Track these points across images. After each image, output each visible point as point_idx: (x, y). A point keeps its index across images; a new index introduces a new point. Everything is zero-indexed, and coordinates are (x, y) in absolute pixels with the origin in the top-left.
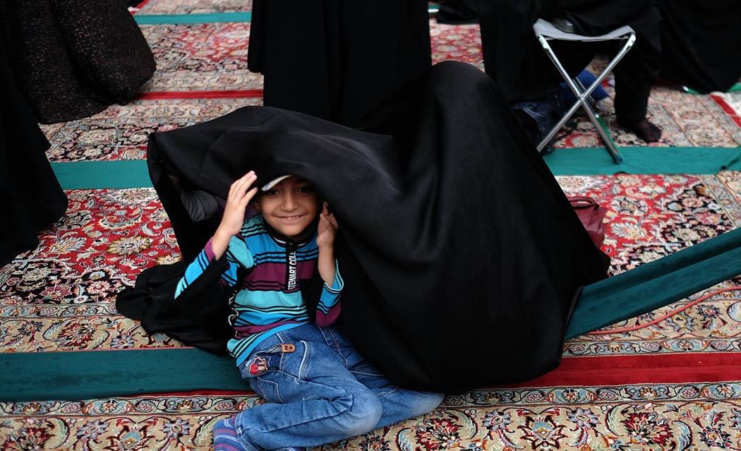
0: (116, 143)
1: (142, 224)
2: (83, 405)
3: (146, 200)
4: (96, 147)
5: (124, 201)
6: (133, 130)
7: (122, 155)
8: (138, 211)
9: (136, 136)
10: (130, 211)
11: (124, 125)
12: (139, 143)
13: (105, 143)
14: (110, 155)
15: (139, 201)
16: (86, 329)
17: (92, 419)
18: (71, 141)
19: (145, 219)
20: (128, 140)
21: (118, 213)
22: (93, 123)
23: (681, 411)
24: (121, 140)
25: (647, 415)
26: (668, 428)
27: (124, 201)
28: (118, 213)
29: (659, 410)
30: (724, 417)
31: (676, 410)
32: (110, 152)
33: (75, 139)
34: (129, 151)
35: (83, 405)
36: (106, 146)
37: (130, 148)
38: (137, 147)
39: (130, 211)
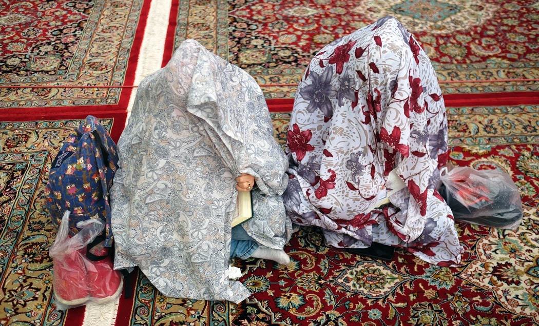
0: (30, 57)
1: (9, 5)
2: (37, 123)
3: (7, 17)
4: (46, 53)
5: (20, 16)
6: (17, 69)
7: (25, 46)
8: (11, 11)
9: (16, 63)
10: (16, 11)
11: (27, 75)
12: (13, 56)
13: (39, 56)
14: (33, 46)
15: (11, 16)
16: (30, 258)
17: (50, 130)
18: (67, 59)
19: (8, 7)
20: (21, 59)
21: (23, 10)
22: (54, 78)
23: (472, 119)
24: (27, 60)
25: (456, 121)
26: (467, 126)
27: (20, 16)
28: (23, 10)
29: (461, 118)
30: (494, 121)
31: (470, 118)
32: (33, 48)
33: (63, 60)
34: (19, 50)
35: (37, 123)
36: (38, 54)
37: (19, 52)
38: (12, 52)
39: (16, 11)
